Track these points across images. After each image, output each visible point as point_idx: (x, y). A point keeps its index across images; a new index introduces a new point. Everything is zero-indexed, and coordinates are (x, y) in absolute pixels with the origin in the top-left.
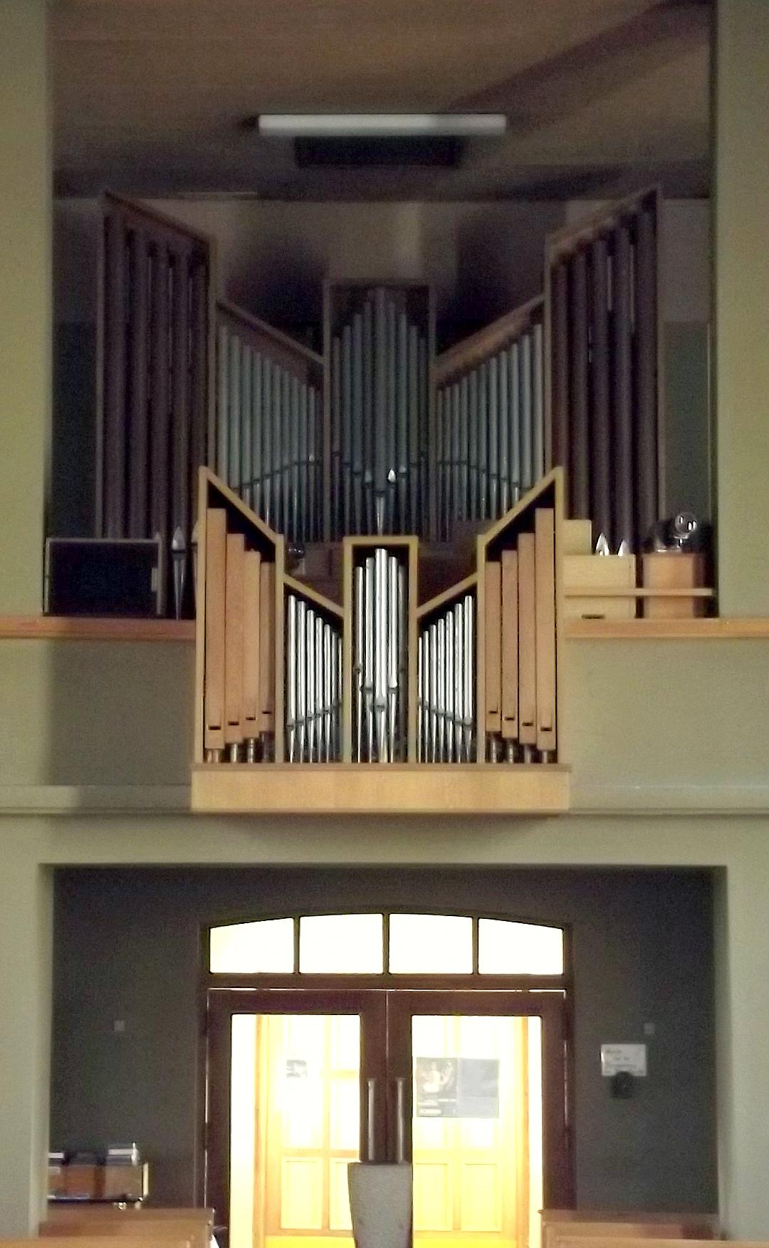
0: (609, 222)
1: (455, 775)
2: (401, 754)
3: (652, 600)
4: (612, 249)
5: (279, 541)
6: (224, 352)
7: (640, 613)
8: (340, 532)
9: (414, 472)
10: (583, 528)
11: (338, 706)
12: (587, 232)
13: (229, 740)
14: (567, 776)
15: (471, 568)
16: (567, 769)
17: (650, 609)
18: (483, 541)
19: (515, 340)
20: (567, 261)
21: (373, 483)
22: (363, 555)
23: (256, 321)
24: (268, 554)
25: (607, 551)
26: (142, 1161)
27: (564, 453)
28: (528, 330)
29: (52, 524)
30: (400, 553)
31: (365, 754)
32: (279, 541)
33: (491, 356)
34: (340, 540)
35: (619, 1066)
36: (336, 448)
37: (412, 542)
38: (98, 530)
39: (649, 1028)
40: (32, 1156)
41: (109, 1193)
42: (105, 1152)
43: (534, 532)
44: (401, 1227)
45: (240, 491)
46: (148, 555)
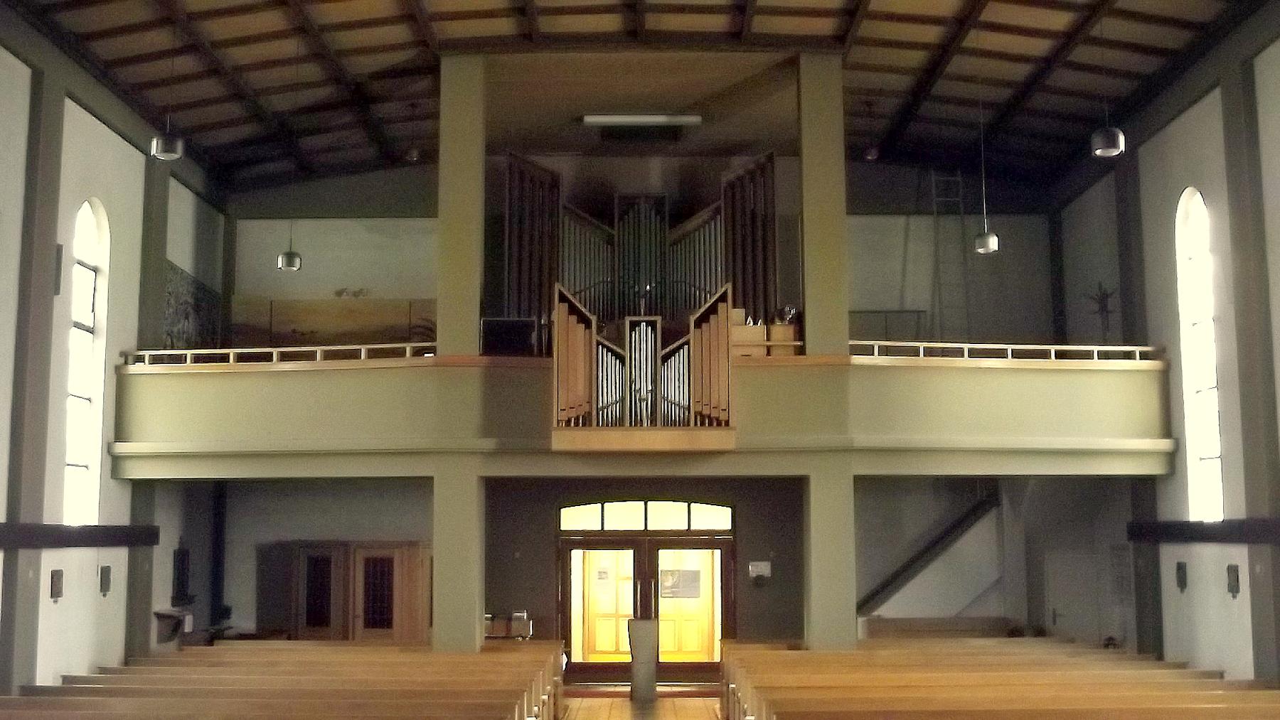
0: (752, 166)
1: (681, 432)
2: (653, 422)
3: (774, 348)
4: (752, 179)
5: (594, 319)
6: (566, 228)
7: (769, 353)
8: (622, 316)
9: (659, 286)
10: (739, 313)
11: (623, 400)
12: (741, 172)
13: (570, 416)
14: (734, 432)
15: (688, 332)
16: (734, 429)
17: (774, 352)
18: (692, 319)
19: (707, 222)
20: (731, 185)
21: (639, 292)
22: (634, 325)
23: (583, 214)
24: (588, 324)
25: (752, 323)
26: (529, 619)
27: (731, 276)
28: (713, 218)
29: (483, 312)
30: (652, 324)
31: (637, 423)
32: (594, 319)
33: (696, 230)
34: (624, 319)
36: (621, 275)
37: (659, 319)
38: (506, 314)
39: (772, 554)
41: (514, 633)
42: (511, 614)
43: (718, 314)
44: (653, 649)
45: (574, 295)
46: (529, 326)
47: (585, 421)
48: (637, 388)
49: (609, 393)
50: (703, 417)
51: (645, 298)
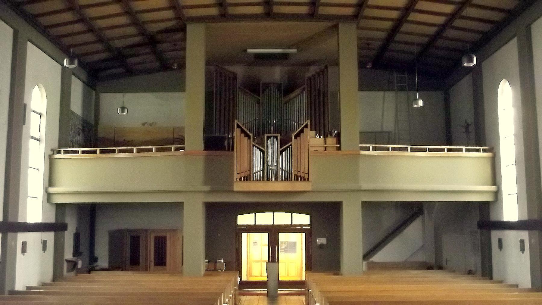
5: (251, 135)
11: (264, 169)
24: (249, 137)
37: (279, 135)
47: (248, 178)
48: (270, 164)
49: (258, 167)
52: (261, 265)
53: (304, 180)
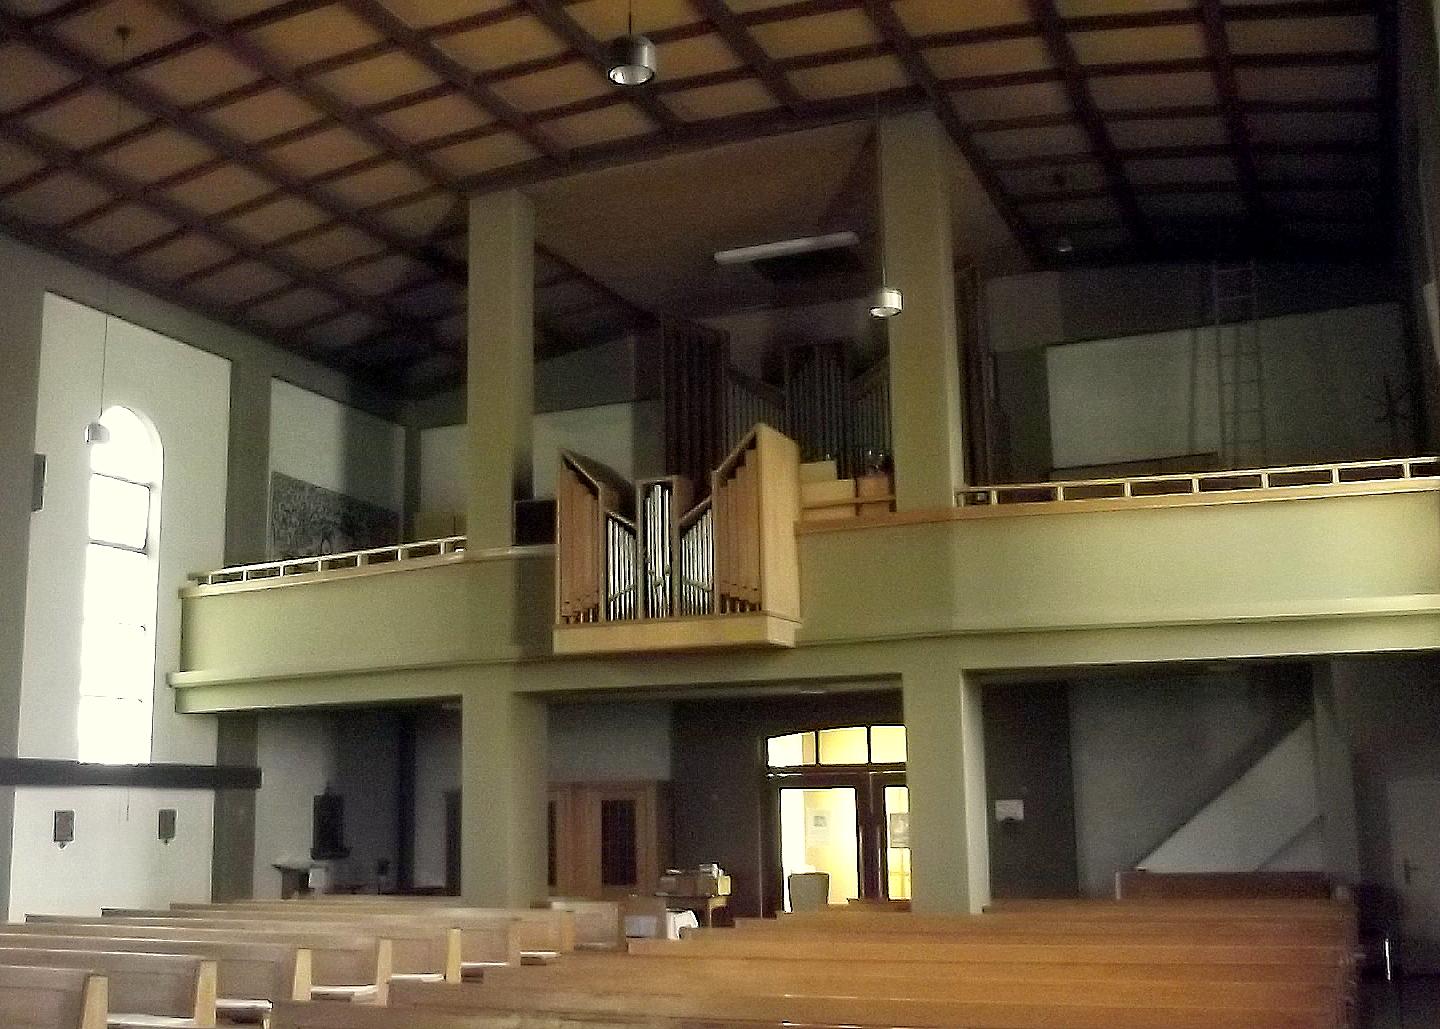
11: (636, 587)
24: (594, 491)
31: (649, 612)
35: (313, 904)
37: (673, 478)
40: (760, 876)
47: (591, 615)
49: (621, 577)
50: (734, 600)
51: (838, 458)
52: (903, 880)
53: (753, 609)
